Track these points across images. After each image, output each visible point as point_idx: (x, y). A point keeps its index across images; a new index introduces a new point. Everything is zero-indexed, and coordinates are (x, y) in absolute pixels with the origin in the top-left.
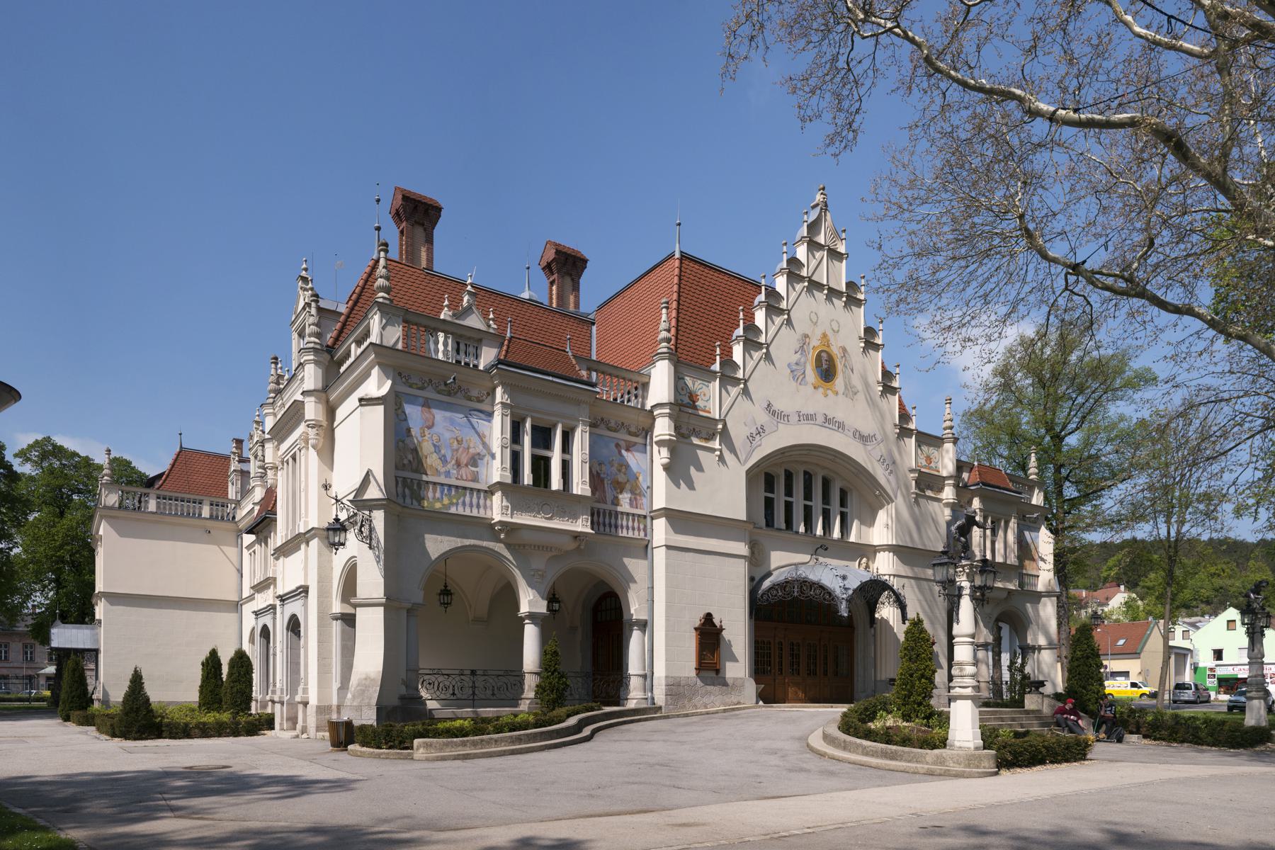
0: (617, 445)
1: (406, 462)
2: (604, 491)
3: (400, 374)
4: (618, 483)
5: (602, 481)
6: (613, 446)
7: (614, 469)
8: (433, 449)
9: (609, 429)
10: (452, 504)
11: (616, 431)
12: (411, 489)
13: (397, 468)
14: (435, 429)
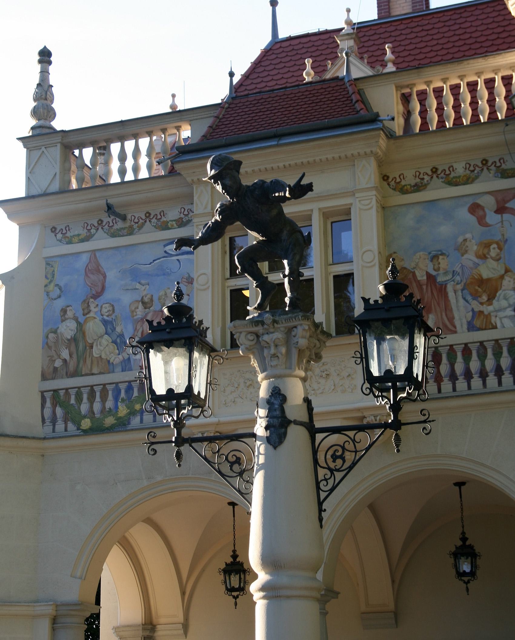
0: (475, 208)
1: (58, 363)
2: (447, 308)
3: (54, 230)
4: (481, 282)
5: (442, 289)
6: (463, 213)
7: (470, 258)
8: (102, 329)
9: (403, 191)
10: (132, 413)
11: (418, 188)
12: (65, 405)
13: (44, 378)
14: (108, 295)
